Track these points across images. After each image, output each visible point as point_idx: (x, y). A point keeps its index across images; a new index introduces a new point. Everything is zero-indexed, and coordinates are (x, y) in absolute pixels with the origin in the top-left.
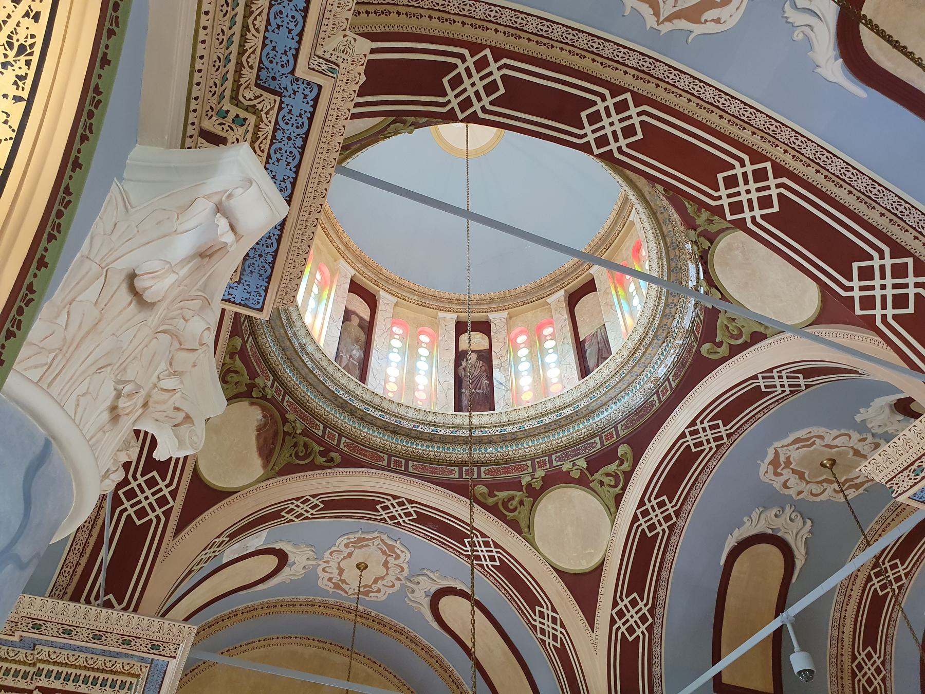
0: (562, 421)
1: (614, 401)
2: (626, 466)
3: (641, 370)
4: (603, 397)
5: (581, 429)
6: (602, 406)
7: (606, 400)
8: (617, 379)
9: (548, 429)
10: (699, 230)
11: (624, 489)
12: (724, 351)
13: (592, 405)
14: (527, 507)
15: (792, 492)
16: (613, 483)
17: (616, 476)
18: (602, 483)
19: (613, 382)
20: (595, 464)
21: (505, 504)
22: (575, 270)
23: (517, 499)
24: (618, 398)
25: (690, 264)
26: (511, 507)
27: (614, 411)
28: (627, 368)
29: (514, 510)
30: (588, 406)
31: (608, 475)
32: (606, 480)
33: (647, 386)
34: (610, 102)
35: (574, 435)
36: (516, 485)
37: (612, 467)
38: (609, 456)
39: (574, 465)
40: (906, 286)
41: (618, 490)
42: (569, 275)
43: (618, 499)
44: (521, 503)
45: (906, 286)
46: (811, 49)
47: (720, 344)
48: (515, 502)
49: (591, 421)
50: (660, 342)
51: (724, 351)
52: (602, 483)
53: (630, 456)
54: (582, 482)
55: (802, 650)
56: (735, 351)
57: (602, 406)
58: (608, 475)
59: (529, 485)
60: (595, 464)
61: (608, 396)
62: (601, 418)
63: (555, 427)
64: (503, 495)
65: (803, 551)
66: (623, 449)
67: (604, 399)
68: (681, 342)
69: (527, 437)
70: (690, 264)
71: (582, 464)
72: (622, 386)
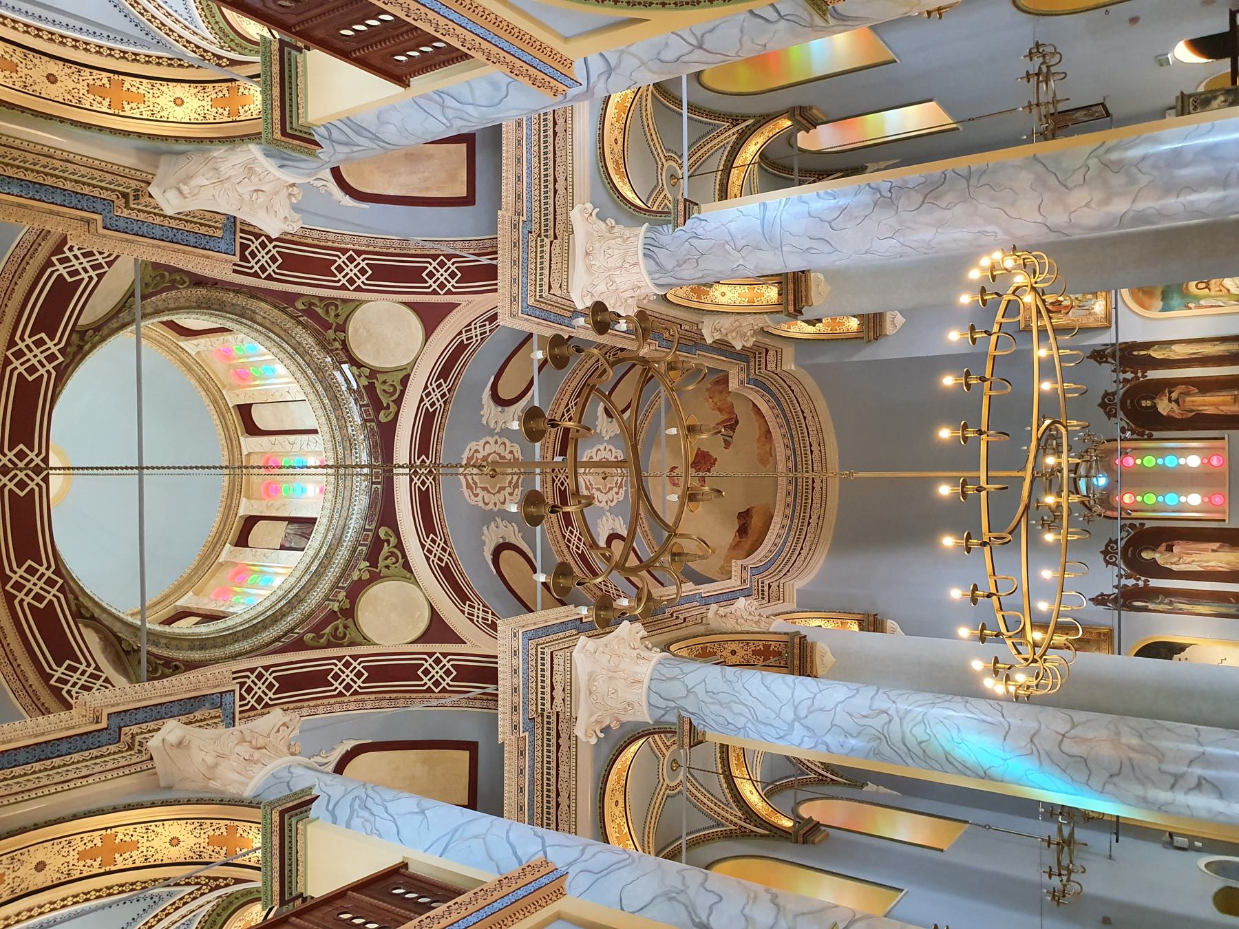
0: (324, 561)
1: (349, 518)
2: (393, 541)
3: (350, 482)
4: (346, 492)
5: (343, 554)
6: (344, 529)
7: (343, 522)
8: (340, 500)
9: (318, 574)
10: (334, 327)
11: (404, 556)
12: (393, 408)
13: (337, 532)
14: (352, 626)
15: (491, 506)
16: (394, 560)
17: (393, 554)
18: (387, 567)
19: (338, 505)
20: (373, 558)
21: (335, 635)
22: (225, 525)
23: (341, 626)
24: (350, 514)
25: (335, 373)
26: (341, 635)
27: (355, 523)
28: (341, 488)
29: (345, 635)
30: (334, 535)
31: (386, 558)
32: (388, 562)
33: (363, 487)
34: (21, 596)
35: (341, 561)
36: (332, 616)
37: (386, 549)
38: (377, 544)
39: (360, 570)
40: (430, 680)
41: (401, 561)
42: (222, 532)
43: (407, 566)
44: (346, 627)
45: (430, 680)
46: (332, 195)
47: (388, 407)
48: (341, 629)
49: (345, 544)
50: (349, 451)
51: (393, 408)
52: (387, 567)
53: (390, 532)
54: (375, 578)
55: (532, 359)
56: (399, 402)
57: (344, 529)
58: (386, 558)
59: (341, 610)
60: (373, 558)
61: (342, 518)
62: (350, 535)
63: (323, 570)
64: (328, 630)
65: (527, 546)
66: (382, 532)
67: (341, 523)
68: (363, 437)
69: (308, 593)
70: (335, 373)
71: (364, 564)
72: (346, 504)
